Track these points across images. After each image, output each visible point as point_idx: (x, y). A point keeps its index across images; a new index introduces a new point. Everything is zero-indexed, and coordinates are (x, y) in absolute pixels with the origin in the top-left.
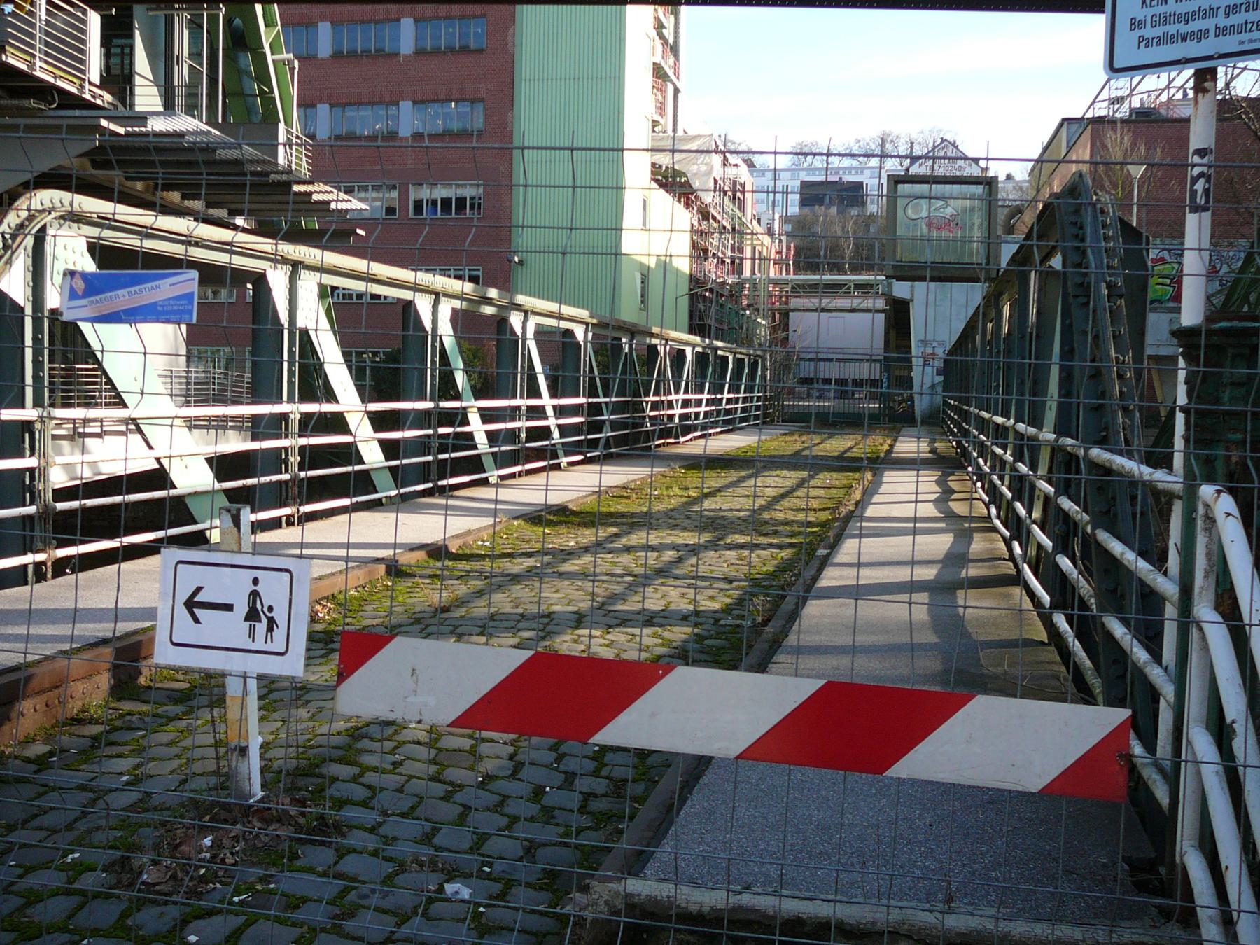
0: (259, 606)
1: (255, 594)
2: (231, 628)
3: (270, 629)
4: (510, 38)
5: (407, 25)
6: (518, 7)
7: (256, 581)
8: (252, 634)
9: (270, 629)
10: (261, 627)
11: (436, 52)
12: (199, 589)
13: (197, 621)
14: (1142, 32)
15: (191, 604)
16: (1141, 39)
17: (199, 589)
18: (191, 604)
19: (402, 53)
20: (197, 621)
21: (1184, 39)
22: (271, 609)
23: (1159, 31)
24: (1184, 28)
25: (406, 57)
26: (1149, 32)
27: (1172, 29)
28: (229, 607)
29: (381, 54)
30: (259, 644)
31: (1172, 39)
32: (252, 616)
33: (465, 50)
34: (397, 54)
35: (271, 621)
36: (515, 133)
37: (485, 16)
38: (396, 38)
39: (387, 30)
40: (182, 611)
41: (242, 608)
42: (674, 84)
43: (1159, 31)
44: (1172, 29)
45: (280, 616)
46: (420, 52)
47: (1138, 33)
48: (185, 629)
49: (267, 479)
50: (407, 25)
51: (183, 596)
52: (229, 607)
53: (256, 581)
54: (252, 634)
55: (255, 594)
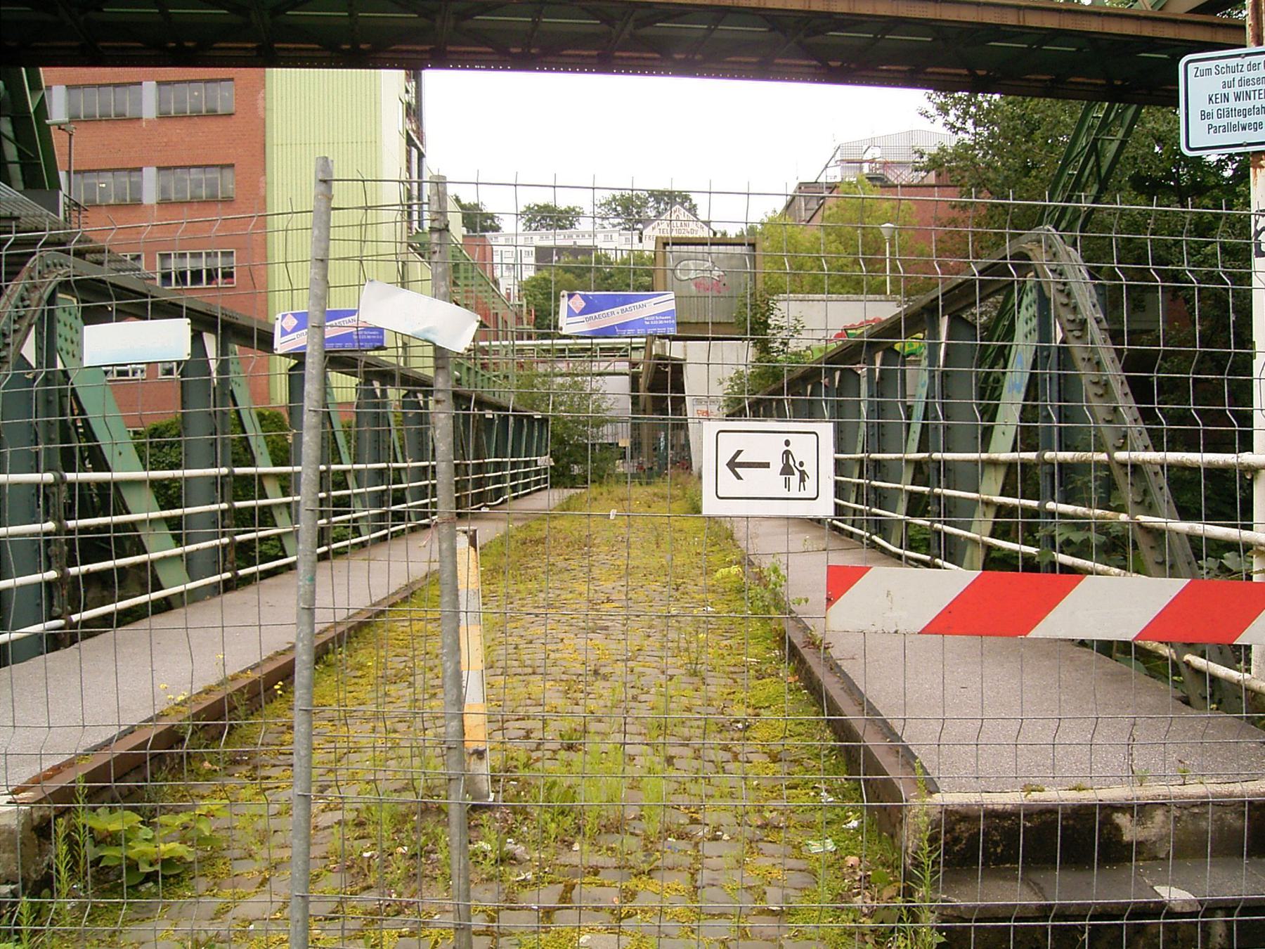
0: (791, 462)
1: (787, 453)
2: (770, 481)
3: (802, 480)
4: (260, 102)
5: (149, 90)
6: (268, 70)
7: (787, 443)
8: (787, 485)
9: (802, 480)
10: (795, 479)
11: (181, 116)
12: (739, 452)
13: (739, 478)
14: (1210, 121)
15: (733, 465)
16: (1210, 127)
17: (739, 452)
18: (733, 465)
19: (144, 117)
20: (739, 478)
21: (1244, 128)
22: (801, 464)
23: (1224, 121)
24: (1243, 121)
25: (148, 121)
26: (1216, 122)
27: (1234, 120)
28: (767, 465)
29: (121, 118)
30: (794, 493)
31: (1234, 128)
32: (787, 470)
33: (212, 114)
34: (140, 119)
35: (803, 473)
36: (268, 200)
37: (232, 79)
38: (138, 102)
39: (126, 95)
40: (725, 471)
41: (777, 465)
42: (418, 149)
43: (1224, 121)
44: (1234, 120)
45: (810, 468)
46: (164, 116)
47: (1207, 122)
48: (728, 483)
49: (21, 580)
50: (149, 90)
51: (725, 457)
52: (767, 465)
53: (787, 443)
54: (787, 485)
55: (787, 453)
